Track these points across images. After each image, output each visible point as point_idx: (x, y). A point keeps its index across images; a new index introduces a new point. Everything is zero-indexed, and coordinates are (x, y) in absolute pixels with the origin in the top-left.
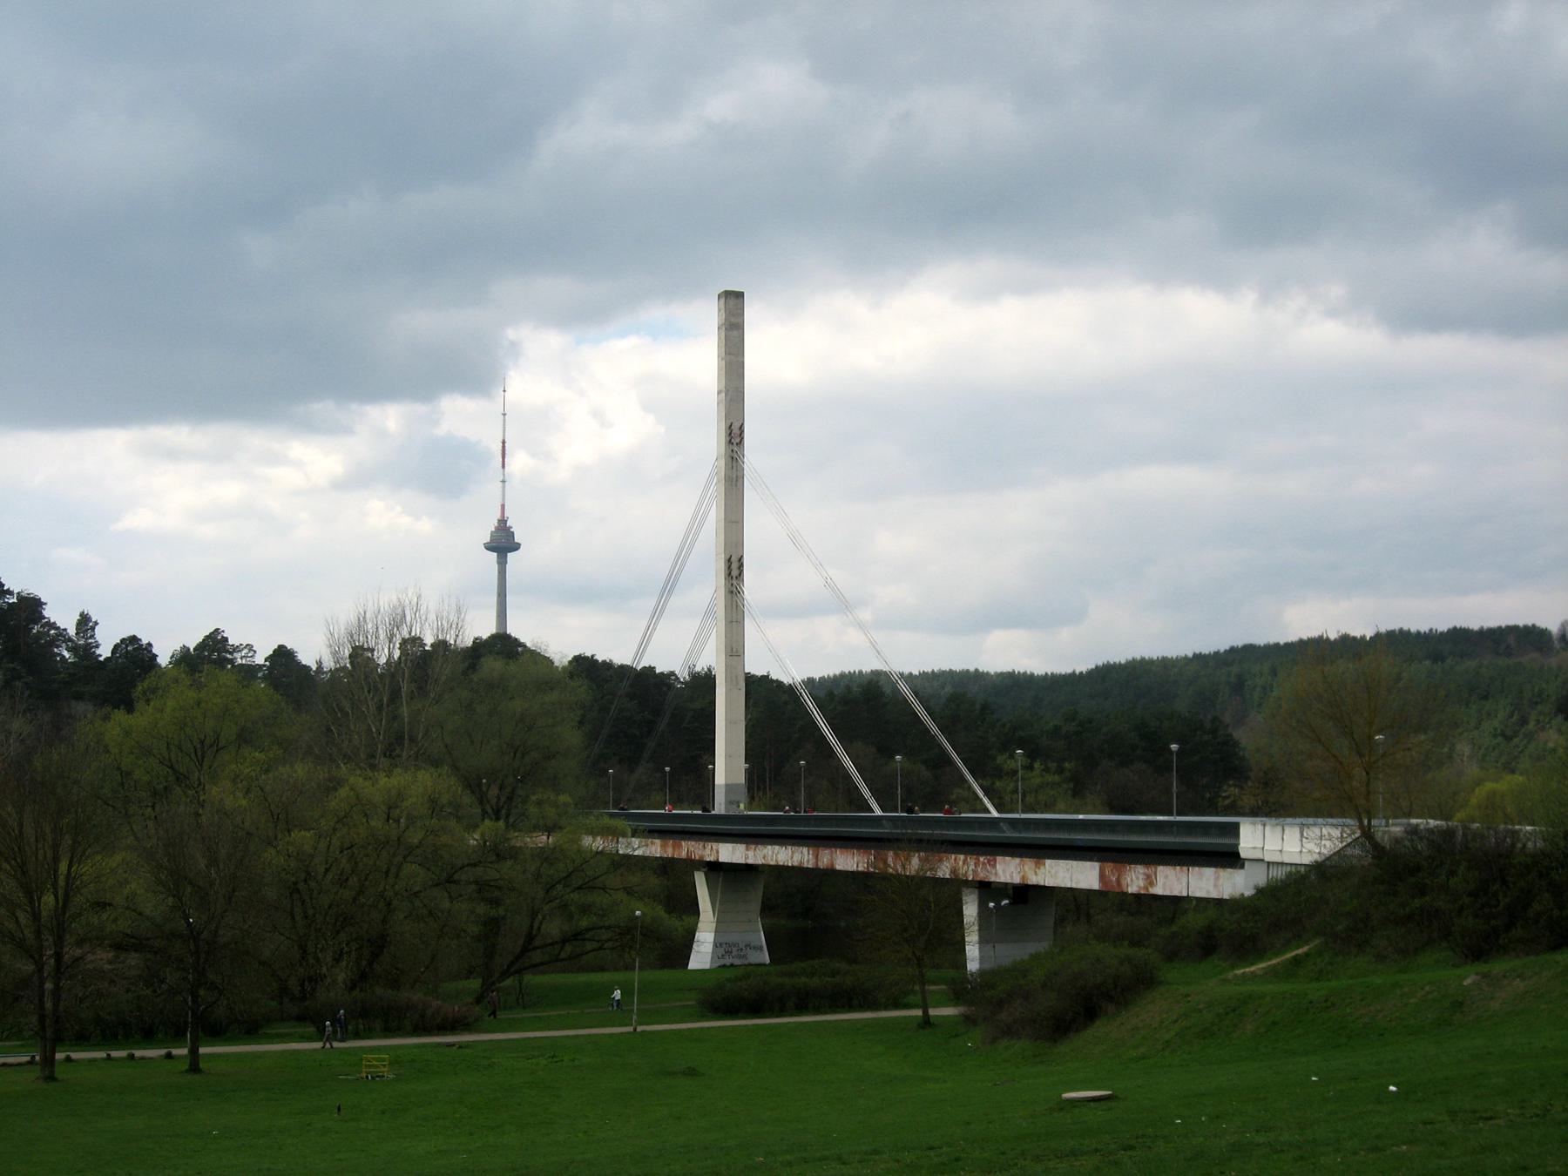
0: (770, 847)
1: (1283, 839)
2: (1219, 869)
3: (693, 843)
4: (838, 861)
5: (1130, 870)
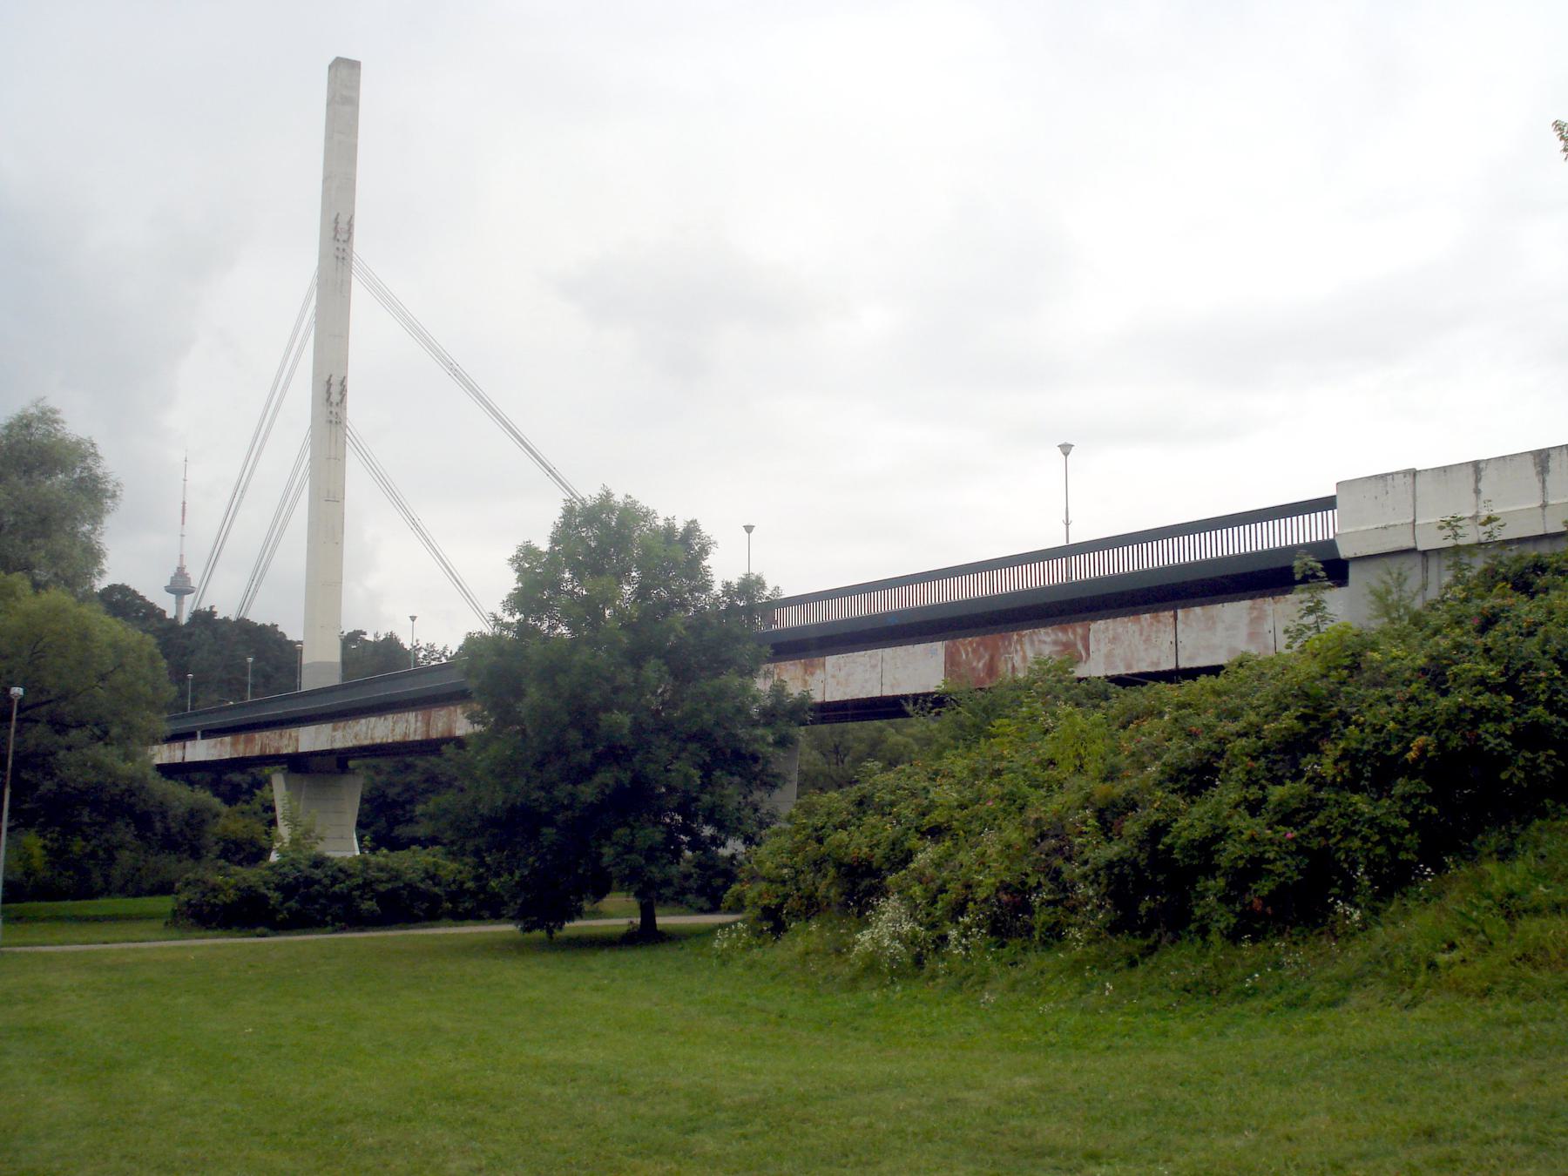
0: (363, 721)
1: (1477, 491)
2: (1259, 601)
3: (268, 733)
4: (458, 724)
5: (1020, 641)
